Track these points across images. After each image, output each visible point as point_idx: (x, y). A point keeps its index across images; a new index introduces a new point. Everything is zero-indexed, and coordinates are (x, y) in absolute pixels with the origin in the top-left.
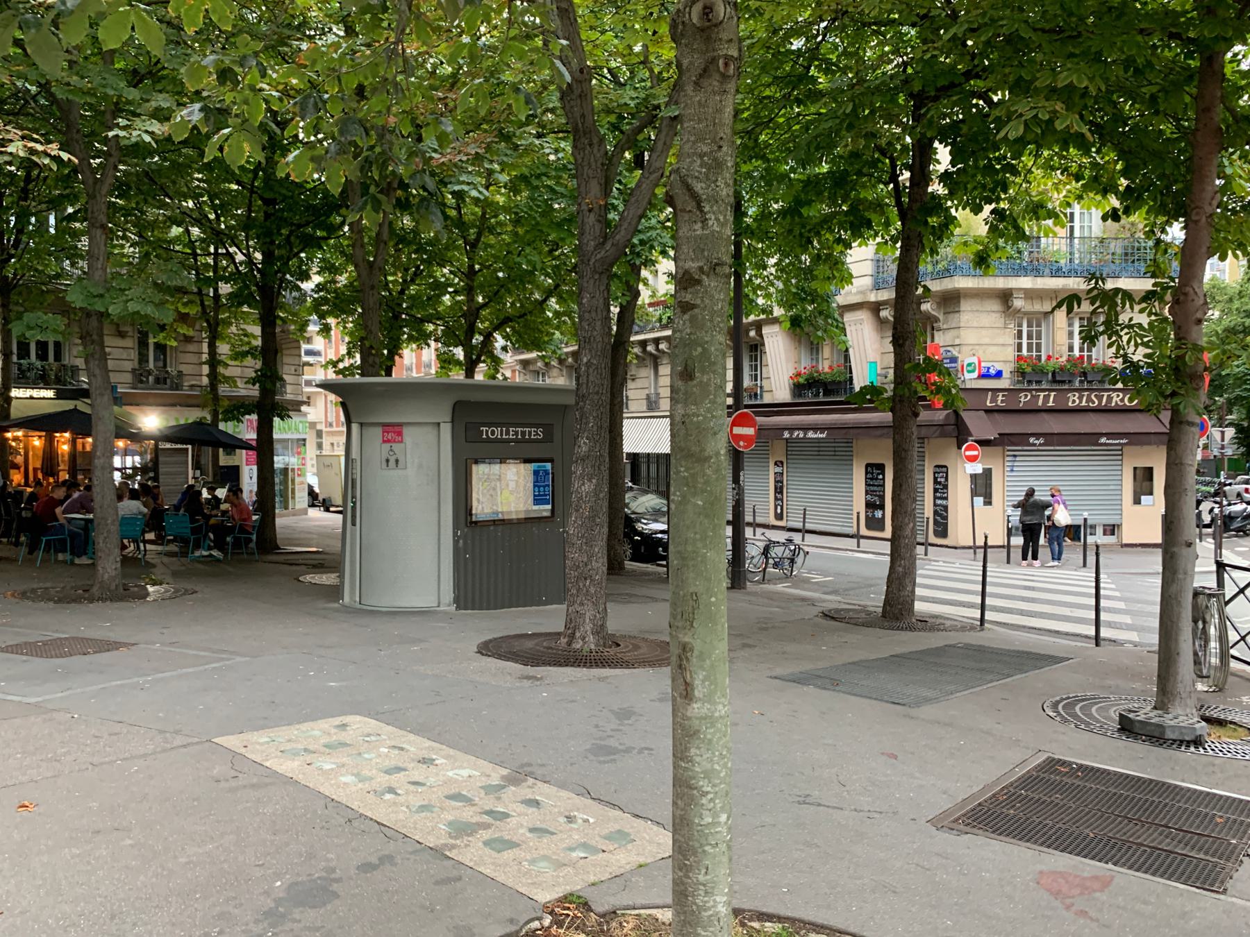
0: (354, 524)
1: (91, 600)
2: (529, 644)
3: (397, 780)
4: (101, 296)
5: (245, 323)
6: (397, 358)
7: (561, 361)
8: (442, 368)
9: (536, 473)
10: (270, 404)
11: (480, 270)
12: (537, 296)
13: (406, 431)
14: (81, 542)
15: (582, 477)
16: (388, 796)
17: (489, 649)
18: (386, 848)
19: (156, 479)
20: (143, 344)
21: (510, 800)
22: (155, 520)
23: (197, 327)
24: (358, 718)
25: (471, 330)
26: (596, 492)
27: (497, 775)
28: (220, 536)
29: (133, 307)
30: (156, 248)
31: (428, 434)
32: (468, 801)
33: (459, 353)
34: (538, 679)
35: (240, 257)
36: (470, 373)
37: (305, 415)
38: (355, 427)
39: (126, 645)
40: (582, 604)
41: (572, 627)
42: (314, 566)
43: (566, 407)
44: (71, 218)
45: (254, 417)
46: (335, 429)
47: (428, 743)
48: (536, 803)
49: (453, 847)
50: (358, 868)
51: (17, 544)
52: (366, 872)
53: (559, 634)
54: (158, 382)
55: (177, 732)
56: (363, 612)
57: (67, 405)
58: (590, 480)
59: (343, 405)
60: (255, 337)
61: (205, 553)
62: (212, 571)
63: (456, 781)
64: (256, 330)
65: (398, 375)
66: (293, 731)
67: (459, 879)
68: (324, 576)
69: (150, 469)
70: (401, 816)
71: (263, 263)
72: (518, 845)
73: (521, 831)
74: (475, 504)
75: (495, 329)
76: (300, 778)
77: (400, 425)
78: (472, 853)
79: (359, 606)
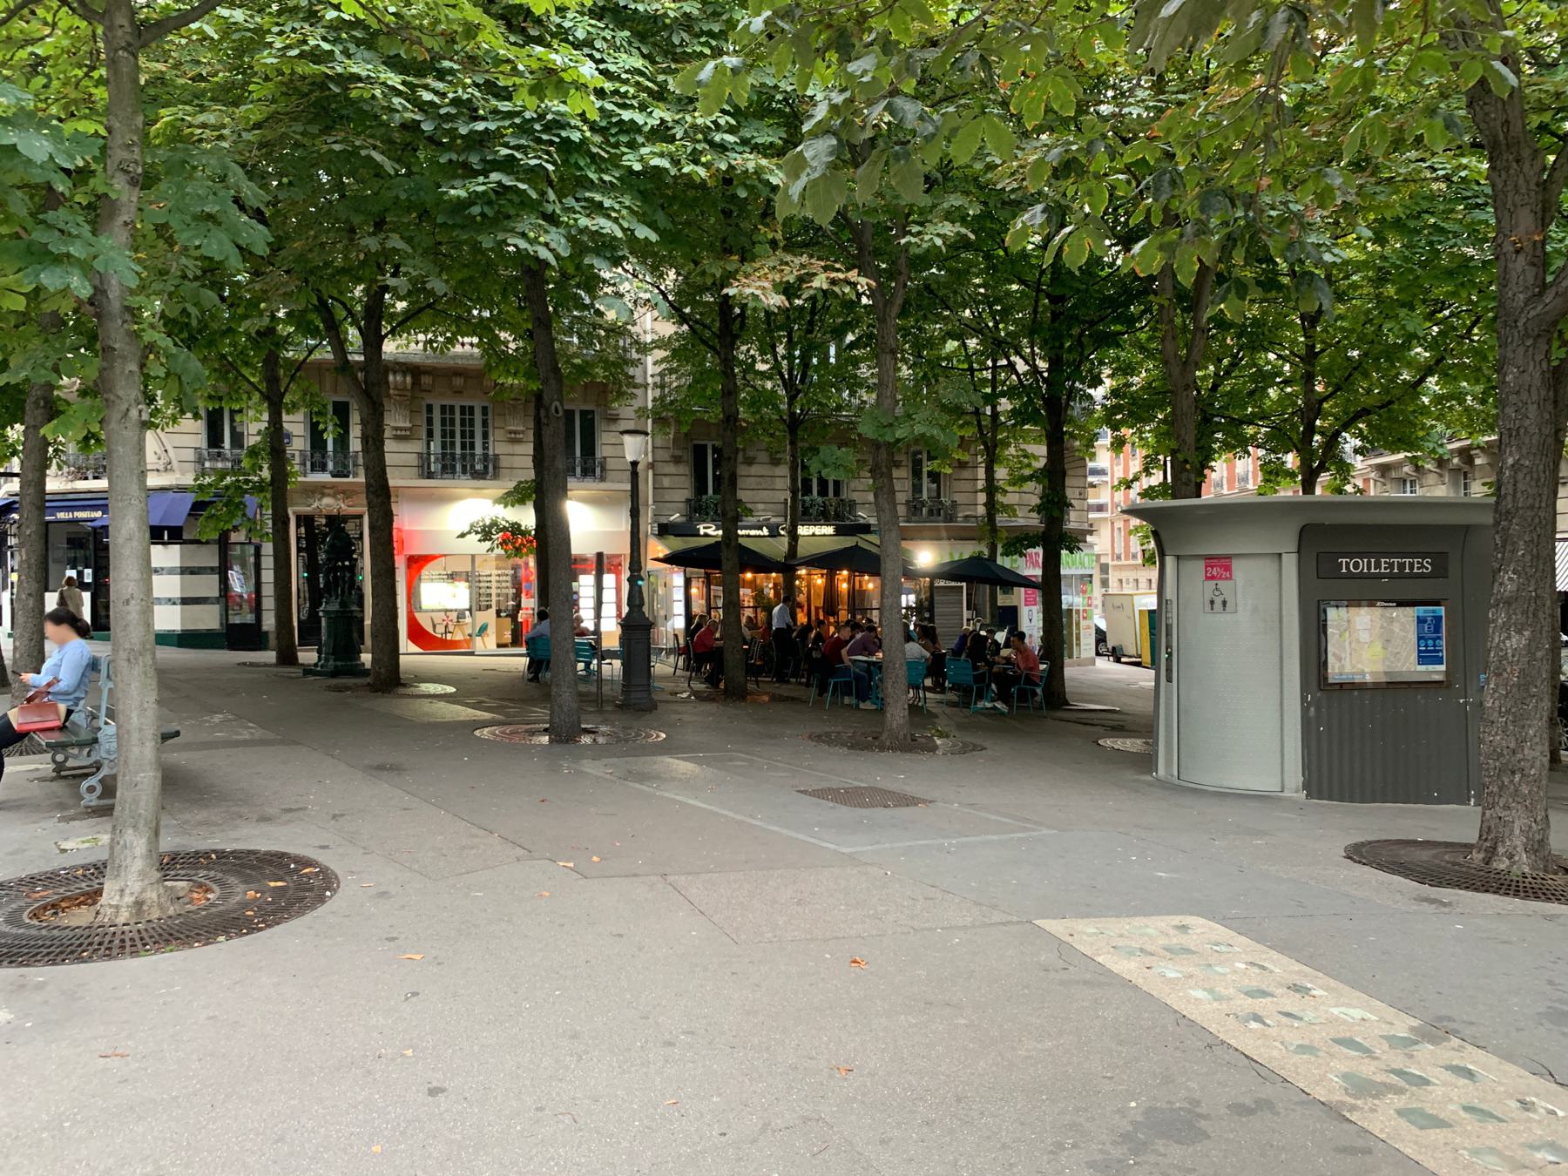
0: (1169, 680)
1: (882, 748)
2: (1425, 855)
3: (1260, 1005)
4: (891, 425)
5: (1025, 442)
6: (1206, 471)
7: (1441, 463)
8: (1266, 481)
9: (1421, 621)
10: (1056, 536)
11: (1323, 351)
12: (1406, 376)
13: (1236, 565)
14: (864, 685)
15: (1506, 627)
16: (1254, 1025)
17: (1360, 854)
18: (1264, 1096)
19: (931, 619)
20: (917, 473)
21: (1428, 1059)
22: (936, 666)
23: (972, 451)
24: (1201, 921)
25: (1311, 430)
26: (1531, 648)
27: (1403, 1025)
28: (1004, 688)
29: (919, 429)
30: (932, 371)
31: (1267, 569)
32: (1367, 1052)
33: (1291, 460)
34: (1445, 905)
35: (1021, 367)
36: (1308, 486)
37: (1091, 546)
38: (1170, 561)
39: (924, 801)
40: (1507, 807)
41: (1490, 841)
42: (1113, 728)
43: (1467, 529)
44: (852, 345)
45: (1039, 550)
46: (1123, 562)
47: (1298, 967)
48: (1469, 1074)
49: (1353, 1108)
50: (1229, 1107)
51: (808, 685)
52: (1240, 1115)
53: (1468, 847)
54: (933, 515)
55: (994, 907)
56: (1180, 789)
57: (848, 542)
58: (1519, 632)
59: (1156, 534)
60: (1036, 458)
61: (989, 705)
62: (996, 725)
63: (1344, 1022)
64: (1042, 450)
65: (1208, 495)
66: (1126, 925)
67: (1370, 1152)
68: (1128, 741)
69: (925, 608)
70: (1275, 1053)
71: (1048, 370)
72: (1451, 1126)
73: (1451, 1107)
74: (1331, 659)
75: (1345, 427)
76: (1140, 982)
77: (1229, 557)
78: (1381, 1119)
79: (1176, 781)
